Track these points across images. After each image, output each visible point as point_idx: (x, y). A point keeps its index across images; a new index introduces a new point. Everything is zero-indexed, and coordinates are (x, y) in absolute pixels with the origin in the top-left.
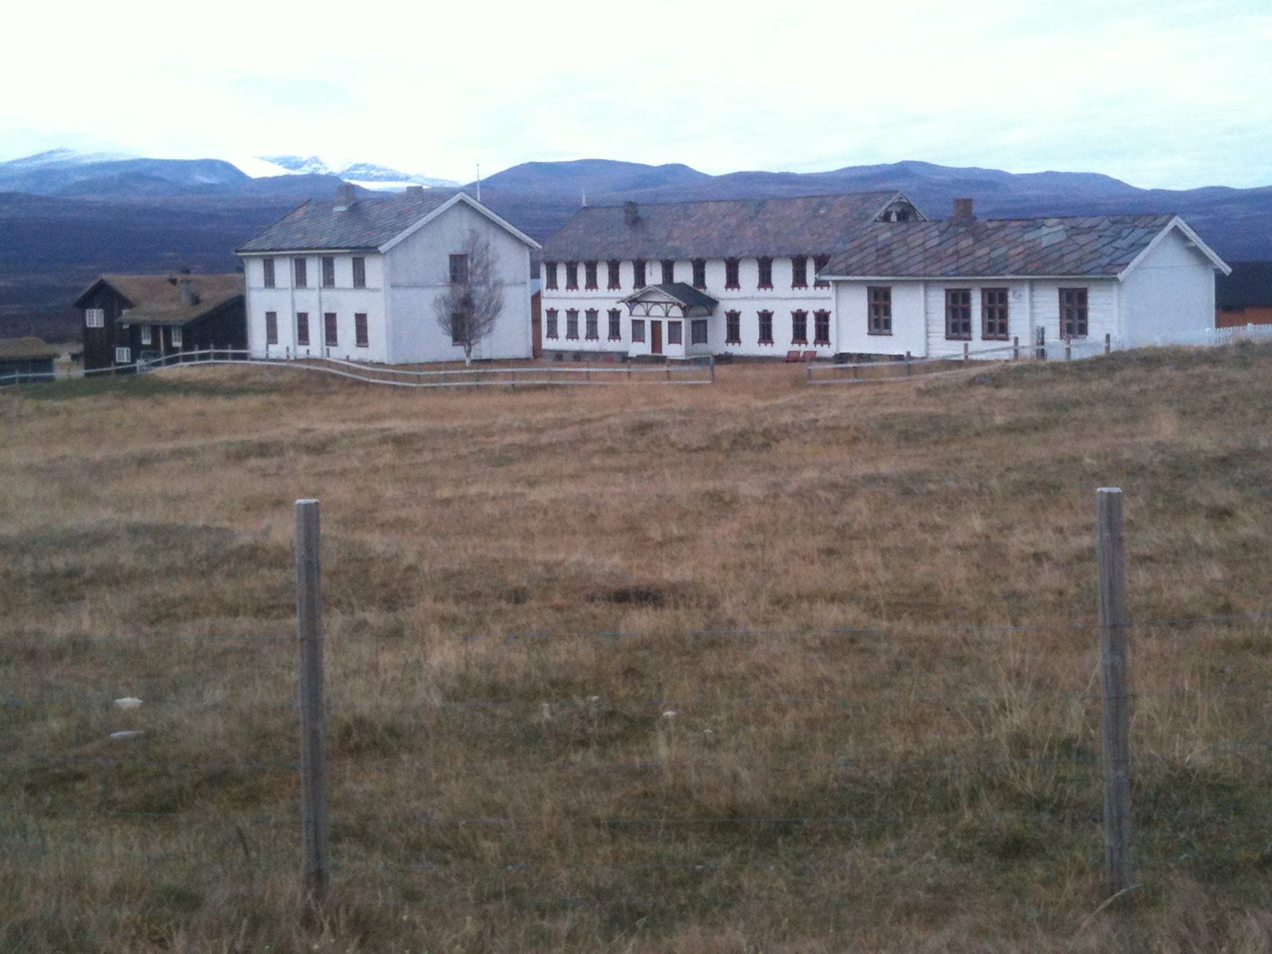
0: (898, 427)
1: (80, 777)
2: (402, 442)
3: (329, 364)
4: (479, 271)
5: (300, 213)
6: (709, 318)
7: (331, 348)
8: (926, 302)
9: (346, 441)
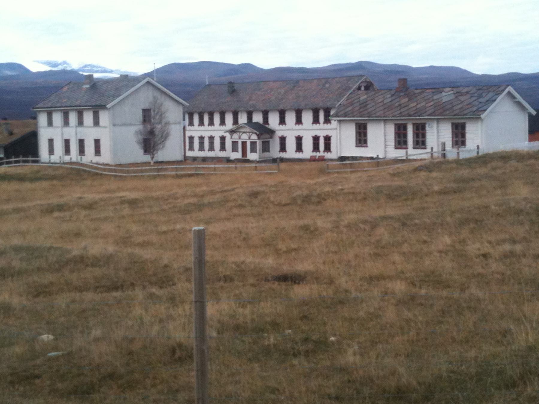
0: (385, 192)
1: (38, 377)
2: (133, 203)
3: (82, 165)
4: (158, 117)
5: (65, 89)
6: (271, 140)
7: (83, 157)
8: (385, 130)
9: (103, 203)
